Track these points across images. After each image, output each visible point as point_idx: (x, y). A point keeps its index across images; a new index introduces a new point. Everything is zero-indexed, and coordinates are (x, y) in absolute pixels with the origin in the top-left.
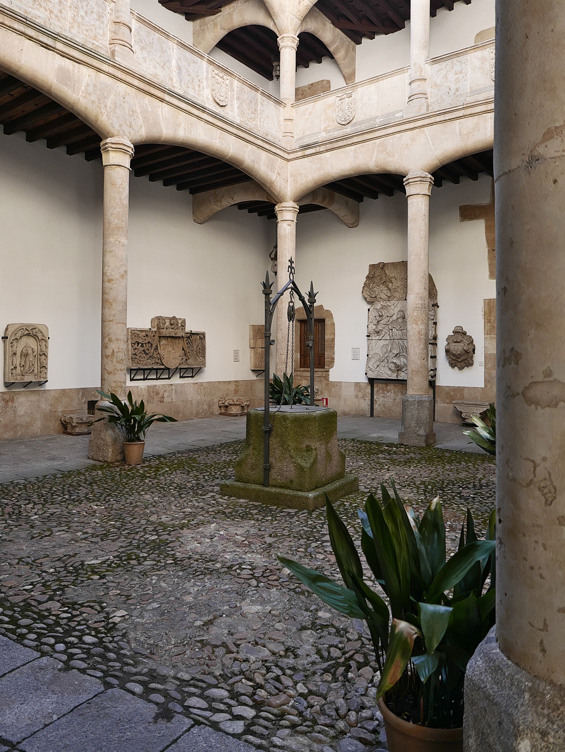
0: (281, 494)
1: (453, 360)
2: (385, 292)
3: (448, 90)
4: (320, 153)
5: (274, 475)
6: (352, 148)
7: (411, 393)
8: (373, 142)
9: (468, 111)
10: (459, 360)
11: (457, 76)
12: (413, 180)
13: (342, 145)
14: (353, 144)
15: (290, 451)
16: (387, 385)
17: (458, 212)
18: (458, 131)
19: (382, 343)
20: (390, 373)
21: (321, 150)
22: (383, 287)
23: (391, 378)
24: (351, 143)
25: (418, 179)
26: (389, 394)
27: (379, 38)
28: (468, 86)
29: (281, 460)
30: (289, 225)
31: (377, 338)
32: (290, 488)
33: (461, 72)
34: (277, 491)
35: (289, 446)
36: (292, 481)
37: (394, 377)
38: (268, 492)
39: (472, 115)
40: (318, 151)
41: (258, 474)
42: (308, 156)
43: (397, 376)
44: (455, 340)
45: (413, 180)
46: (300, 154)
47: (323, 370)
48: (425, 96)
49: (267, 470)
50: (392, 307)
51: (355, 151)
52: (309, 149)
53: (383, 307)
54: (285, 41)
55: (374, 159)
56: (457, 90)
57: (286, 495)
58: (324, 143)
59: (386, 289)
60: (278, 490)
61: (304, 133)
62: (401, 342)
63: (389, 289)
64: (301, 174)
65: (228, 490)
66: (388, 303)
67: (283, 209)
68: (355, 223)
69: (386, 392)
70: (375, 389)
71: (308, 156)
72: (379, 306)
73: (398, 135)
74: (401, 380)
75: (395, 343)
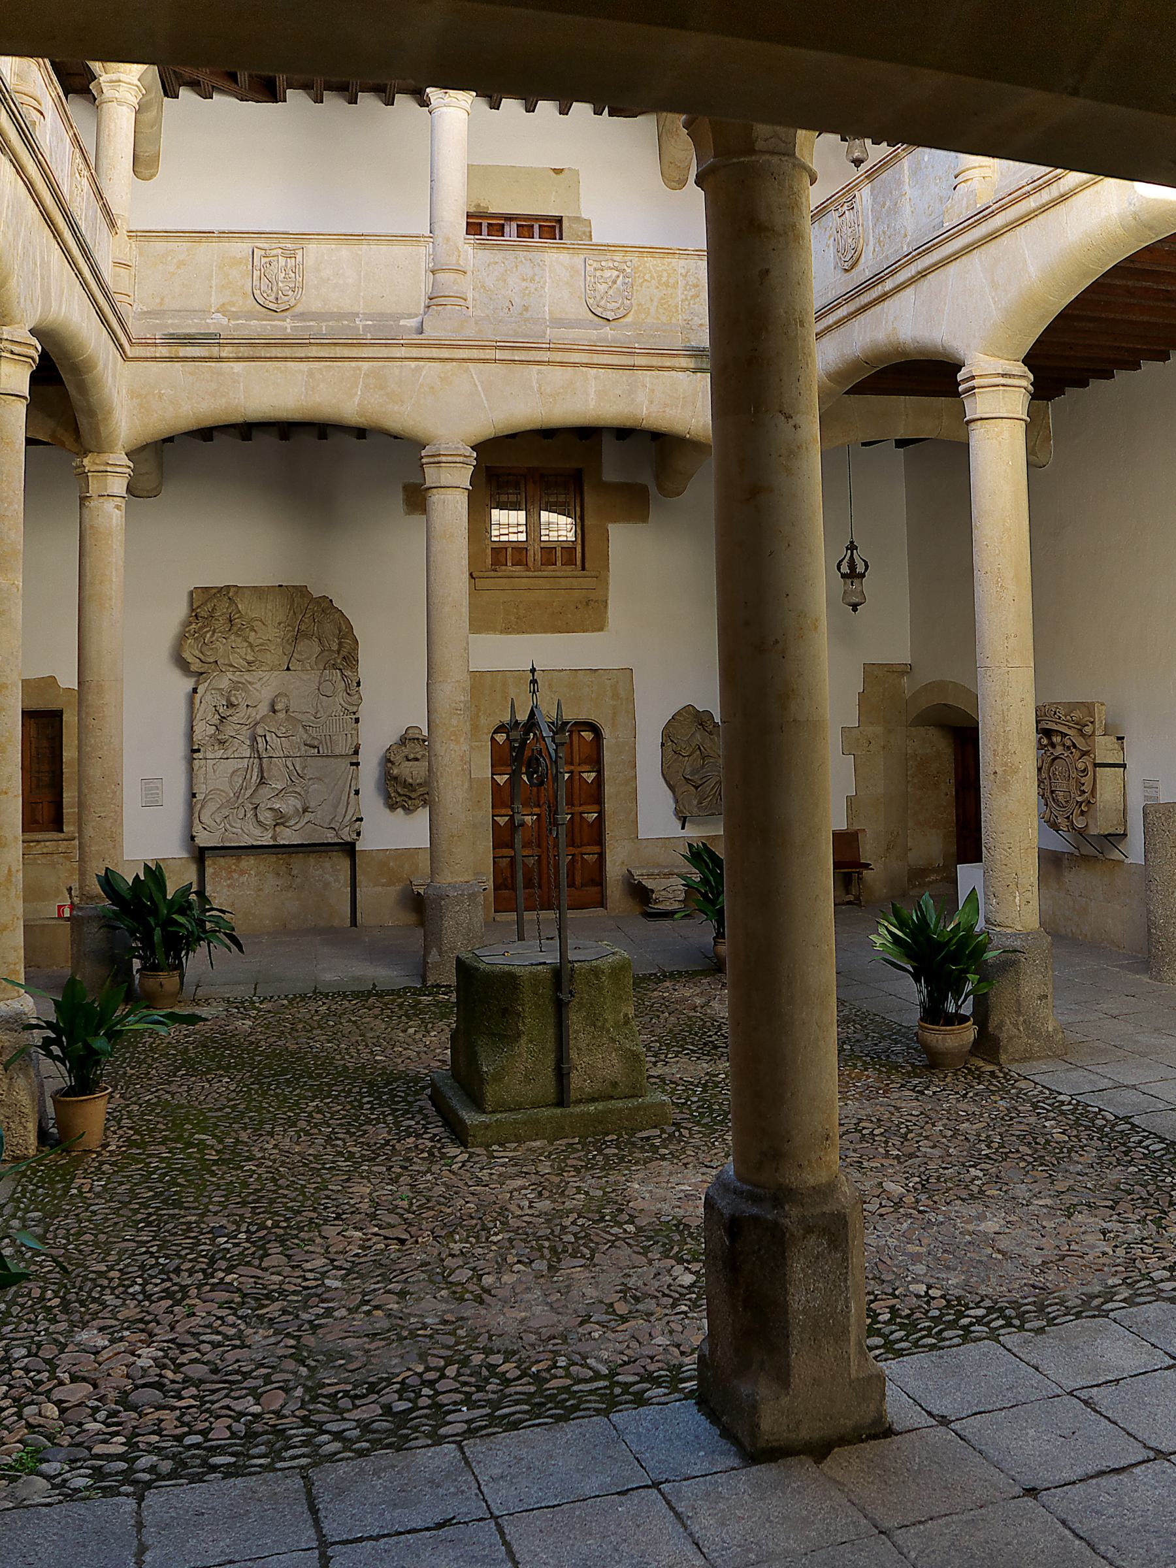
0: (610, 1111)
1: (400, 795)
2: (242, 652)
3: (507, 304)
4: (220, 359)
5: (578, 1082)
6: (304, 366)
7: (449, 880)
8: (353, 364)
9: (558, 356)
10: (413, 795)
11: (524, 284)
12: (450, 459)
13: (279, 355)
14: (307, 359)
15: (608, 1031)
16: (239, 858)
17: (400, 496)
18: (536, 386)
19: (233, 765)
20: (257, 831)
21: (223, 354)
22: (239, 640)
23: (259, 843)
24: (303, 355)
25: (461, 459)
26: (245, 878)
27: (223, 103)
28: (547, 309)
29: (591, 1050)
30: (118, 507)
31: (220, 753)
32: (612, 1098)
33: (532, 280)
34: (600, 1108)
35: (606, 1020)
36: (615, 1085)
37: (267, 840)
38: (583, 1114)
39: (562, 364)
40: (216, 354)
41: (546, 1084)
42: (185, 359)
43: (274, 838)
44: (412, 756)
45: (450, 459)
46: (164, 351)
47: (62, 835)
48: (461, 302)
49: (561, 1076)
50: (258, 686)
51: (311, 373)
52: (188, 343)
53: (236, 686)
54: (121, 89)
55: (357, 400)
56: (526, 308)
57: (621, 1110)
58: (234, 342)
59: (246, 644)
60: (600, 1106)
61: (161, 304)
62: (290, 764)
63: (251, 645)
64: (161, 396)
65: (489, 1133)
66: (247, 676)
67: (109, 469)
68: (155, 489)
69: (236, 876)
70: (209, 871)
71: (185, 359)
72: (224, 684)
73: (413, 364)
74: (284, 846)
75: (276, 764)
